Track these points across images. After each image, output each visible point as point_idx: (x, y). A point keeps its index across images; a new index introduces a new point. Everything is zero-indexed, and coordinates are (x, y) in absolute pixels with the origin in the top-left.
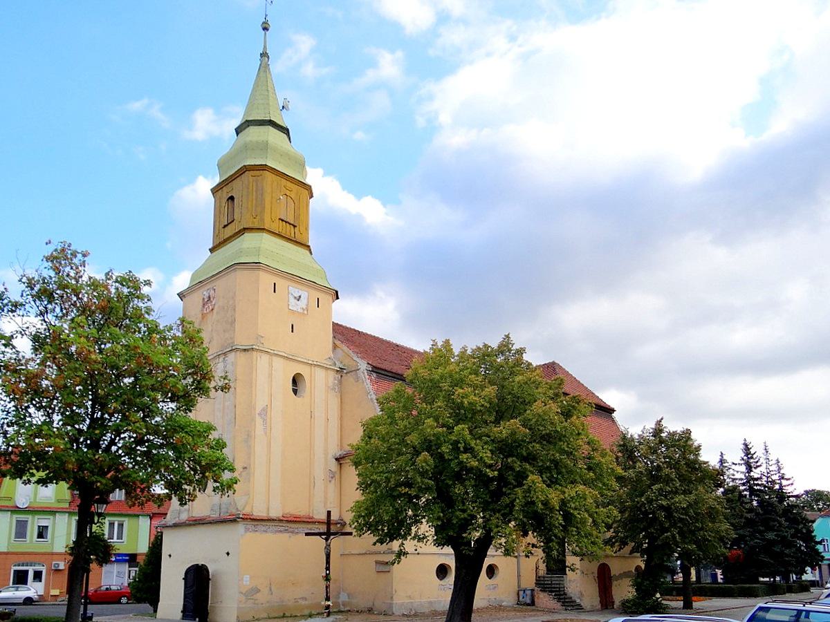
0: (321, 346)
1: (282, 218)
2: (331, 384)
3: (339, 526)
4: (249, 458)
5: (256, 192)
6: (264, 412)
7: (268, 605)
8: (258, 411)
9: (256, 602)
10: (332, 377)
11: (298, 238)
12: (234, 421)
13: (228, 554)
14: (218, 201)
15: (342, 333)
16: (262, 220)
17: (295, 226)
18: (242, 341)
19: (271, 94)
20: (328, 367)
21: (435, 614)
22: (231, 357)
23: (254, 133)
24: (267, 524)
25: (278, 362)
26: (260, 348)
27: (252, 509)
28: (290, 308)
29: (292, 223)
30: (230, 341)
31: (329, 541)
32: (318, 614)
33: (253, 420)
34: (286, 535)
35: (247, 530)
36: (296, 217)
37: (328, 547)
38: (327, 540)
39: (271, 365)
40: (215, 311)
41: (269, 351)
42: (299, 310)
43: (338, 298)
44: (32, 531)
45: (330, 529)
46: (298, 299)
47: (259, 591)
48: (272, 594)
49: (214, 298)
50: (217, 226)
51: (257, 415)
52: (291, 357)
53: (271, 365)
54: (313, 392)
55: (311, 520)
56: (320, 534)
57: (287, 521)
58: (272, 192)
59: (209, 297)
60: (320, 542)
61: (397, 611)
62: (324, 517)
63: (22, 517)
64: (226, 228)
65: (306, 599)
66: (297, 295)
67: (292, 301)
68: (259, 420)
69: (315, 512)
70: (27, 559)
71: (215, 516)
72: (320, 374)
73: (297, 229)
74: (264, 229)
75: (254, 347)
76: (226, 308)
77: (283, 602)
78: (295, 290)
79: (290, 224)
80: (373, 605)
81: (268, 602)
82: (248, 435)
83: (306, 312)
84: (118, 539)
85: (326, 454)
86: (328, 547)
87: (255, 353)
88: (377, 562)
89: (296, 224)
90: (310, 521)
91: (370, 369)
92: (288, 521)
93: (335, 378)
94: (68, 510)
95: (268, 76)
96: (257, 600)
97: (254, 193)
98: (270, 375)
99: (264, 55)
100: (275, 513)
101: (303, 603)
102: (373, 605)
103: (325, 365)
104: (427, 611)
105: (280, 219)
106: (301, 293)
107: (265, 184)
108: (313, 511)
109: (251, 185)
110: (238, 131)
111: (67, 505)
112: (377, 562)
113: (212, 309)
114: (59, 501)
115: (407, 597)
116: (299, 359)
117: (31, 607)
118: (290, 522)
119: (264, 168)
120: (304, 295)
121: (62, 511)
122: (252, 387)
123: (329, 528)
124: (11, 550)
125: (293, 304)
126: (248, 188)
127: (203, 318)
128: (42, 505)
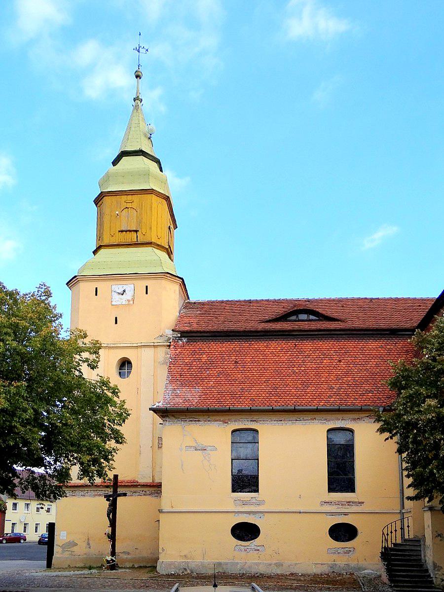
7: (85, 556)
9: (73, 553)
24: (86, 489)
32: (140, 567)
36: (140, 222)
42: (124, 303)
47: (76, 545)
65: (129, 553)
66: (121, 291)
67: (116, 297)
74: (151, 243)
83: (132, 302)
91: (179, 335)
96: (74, 552)
101: (125, 556)
106: (125, 287)
116: (121, 345)
119: (151, 191)
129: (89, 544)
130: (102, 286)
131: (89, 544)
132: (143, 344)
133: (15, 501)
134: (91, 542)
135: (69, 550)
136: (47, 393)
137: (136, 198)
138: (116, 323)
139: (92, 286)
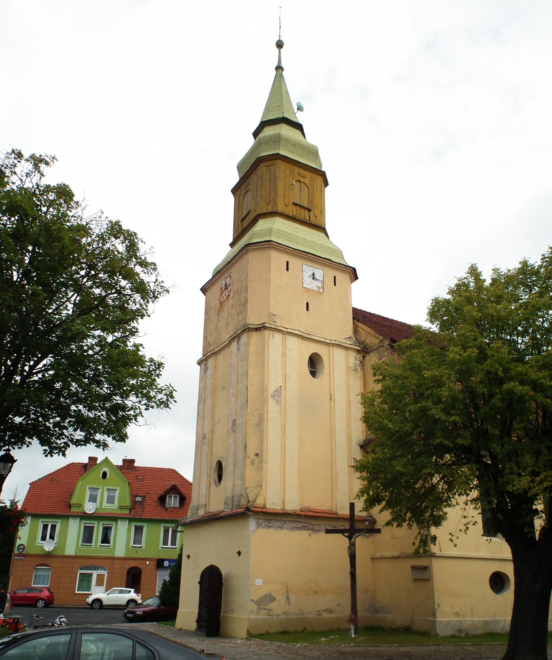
0: (343, 330)
1: (296, 202)
2: (351, 364)
3: (367, 523)
4: (262, 443)
5: (270, 180)
6: (278, 392)
7: (284, 617)
8: (271, 391)
9: (271, 613)
10: (352, 358)
11: (313, 220)
12: (246, 403)
13: (239, 553)
14: (237, 199)
15: (360, 317)
16: (276, 205)
17: (309, 210)
18: (254, 320)
19: (284, 98)
20: (348, 346)
21: (492, 635)
22: (244, 338)
23: (268, 131)
25: (292, 342)
26: (272, 326)
27: (265, 501)
28: (305, 286)
29: (306, 206)
30: (243, 322)
31: (353, 540)
33: (266, 401)
34: (305, 533)
35: (259, 525)
36: (311, 201)
37: (352, 547)
38: (350, 538)
39: (284, 344)
40: (230, 297)
41: (282, 329)
42: (314, 289)
43: (356, 278)
44: (98, 535)
45: (353, 527)
46: (308, 275)
47: (273, 599)
48: (289, 604)
49: (229, 285)
50: (237, 221)
51: (270, 396)
52: (306, 336)
53: (284, 344)
54: (332, 373)
55: (334, 516)
56: (342, 532)
57: (305, 515)
58: (285, 179)
59: (226, 285)
60: (342, 541)
61: (441, 631)
62: (346, 512)
63: (89, 523)
64: (244, 221)
68: (271, 402)
69: (338, 506)
70: (92, 562)
71: (228, 511)
72: (339, 355)
73: (311, 213)
75: (266, 325)
76: (240, 291)
77: (303, 614)
78: (308, 269)
79: (304, 208)
80: (412, 621)
81: (285, 613)
82: (260, 418)
83: (321, 290)
84: (171, 545)
85: (349, 440)
86: (352, 547)
87: (266, 332)
88: (414, 568)
89: (310, 208)
90: (335, 517)
92: (306, 517)
93: (356, 359)
94: (128, 516)
95: (282, 83)
97: (268, 181)
98: (284, 354)
99: (279, 68)
100: (292, 506)
102: (412, 621)
103: (345, 345)
104: (480, 632)
105: (293, 203)
107: (278, 172)
108: (336, 505)
109: (265, 174)
110: (256, 134)
111: (127, 512)
112: (414, 568)
113: (229, 296)
114: (121, 508)
115: (454, 613)
117: (50, 609)
118: (306, 519)
120: (319, 274)
121: (123, 519)
122: (263, 367)
123: (352, 525)
124: (78, 554)
125: (308, 282)
126: (262, 178)
127: (221, 307)
128: (108, 512)
129: (288, 598)
130: (294, 262)
131: (288, 598)
132: (337, 342)
133: (463, 531)
134: (291, 596)
135: (265, 607)
136: (103, 367)
137: (308, 174)
138: (308, 310)
139: (285, 258)
